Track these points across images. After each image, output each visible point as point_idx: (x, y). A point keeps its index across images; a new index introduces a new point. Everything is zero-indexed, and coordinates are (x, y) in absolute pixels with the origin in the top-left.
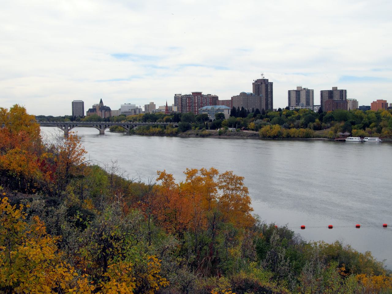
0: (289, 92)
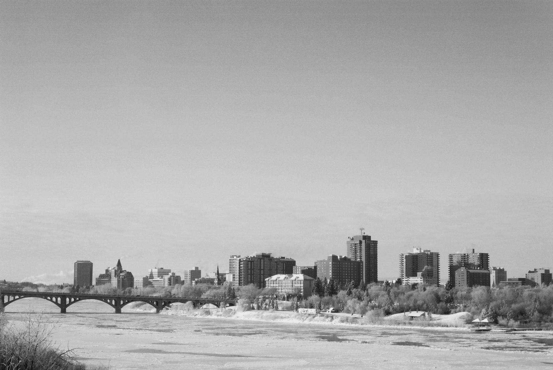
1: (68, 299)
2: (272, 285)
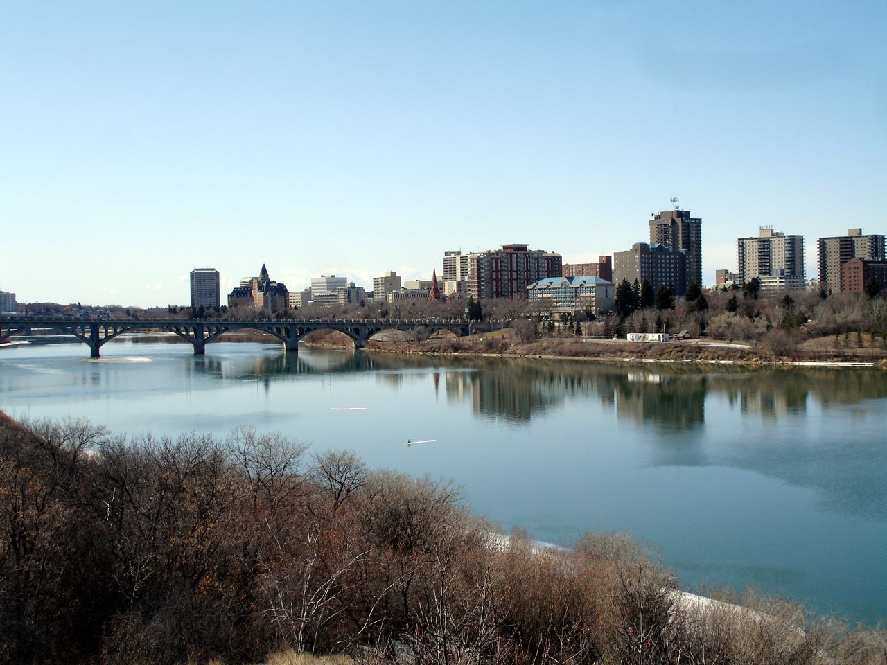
0: (742, 244)
1: (102, 330)
2: (540, 296)
